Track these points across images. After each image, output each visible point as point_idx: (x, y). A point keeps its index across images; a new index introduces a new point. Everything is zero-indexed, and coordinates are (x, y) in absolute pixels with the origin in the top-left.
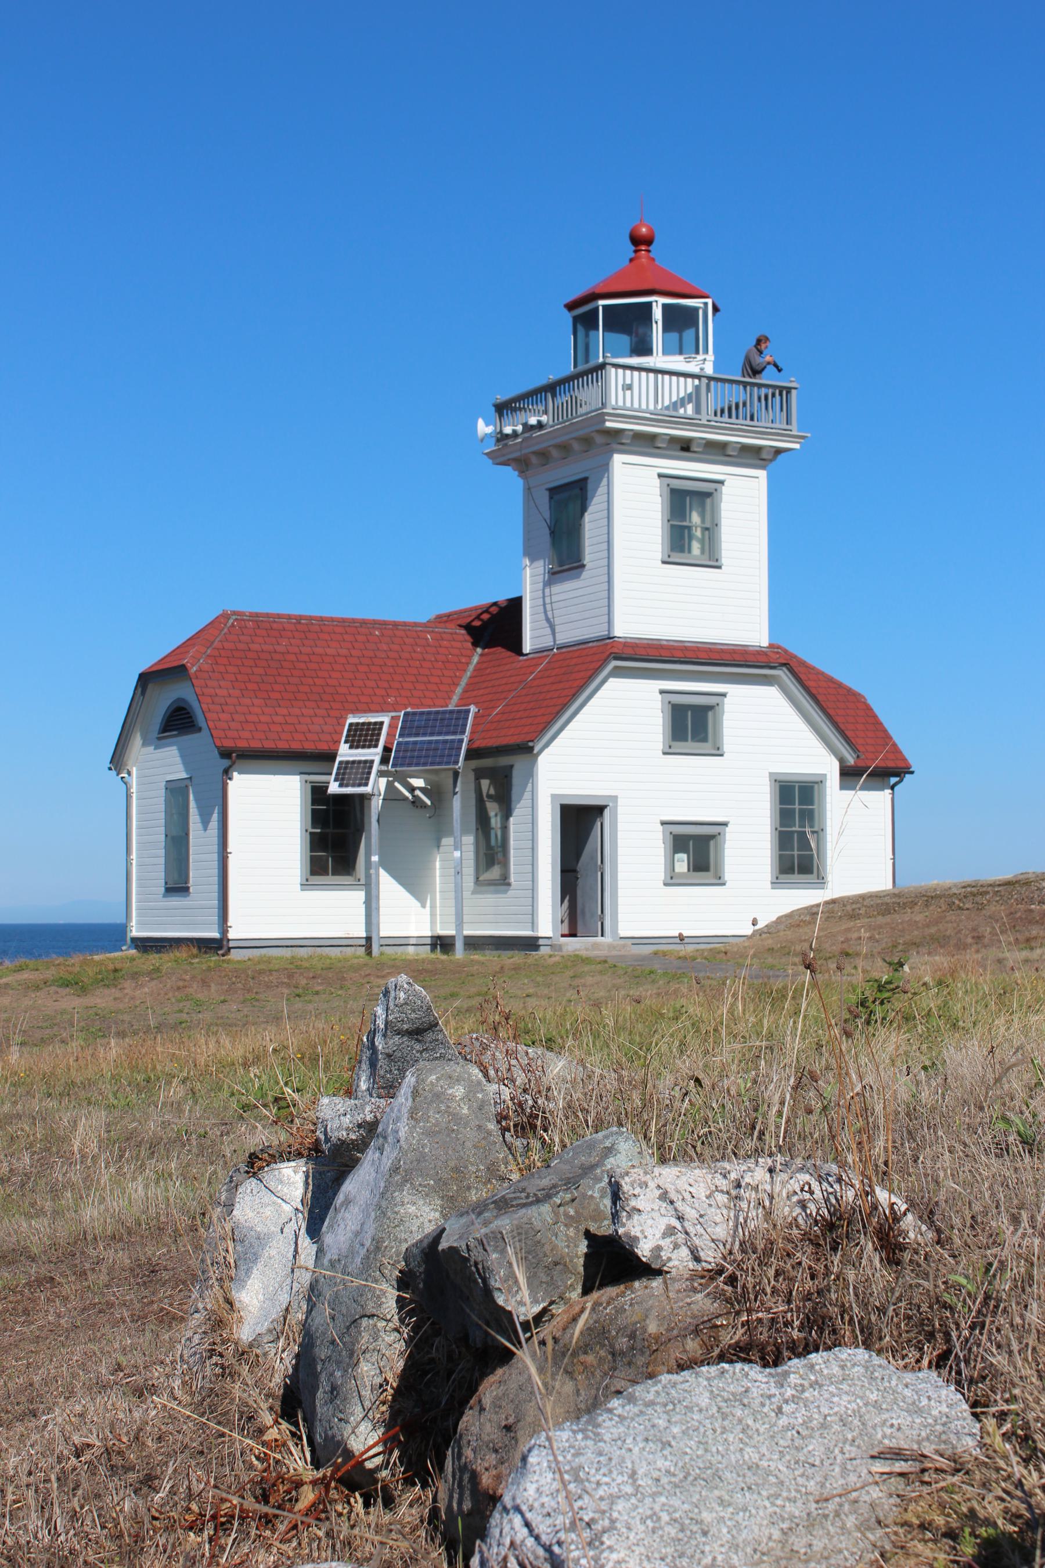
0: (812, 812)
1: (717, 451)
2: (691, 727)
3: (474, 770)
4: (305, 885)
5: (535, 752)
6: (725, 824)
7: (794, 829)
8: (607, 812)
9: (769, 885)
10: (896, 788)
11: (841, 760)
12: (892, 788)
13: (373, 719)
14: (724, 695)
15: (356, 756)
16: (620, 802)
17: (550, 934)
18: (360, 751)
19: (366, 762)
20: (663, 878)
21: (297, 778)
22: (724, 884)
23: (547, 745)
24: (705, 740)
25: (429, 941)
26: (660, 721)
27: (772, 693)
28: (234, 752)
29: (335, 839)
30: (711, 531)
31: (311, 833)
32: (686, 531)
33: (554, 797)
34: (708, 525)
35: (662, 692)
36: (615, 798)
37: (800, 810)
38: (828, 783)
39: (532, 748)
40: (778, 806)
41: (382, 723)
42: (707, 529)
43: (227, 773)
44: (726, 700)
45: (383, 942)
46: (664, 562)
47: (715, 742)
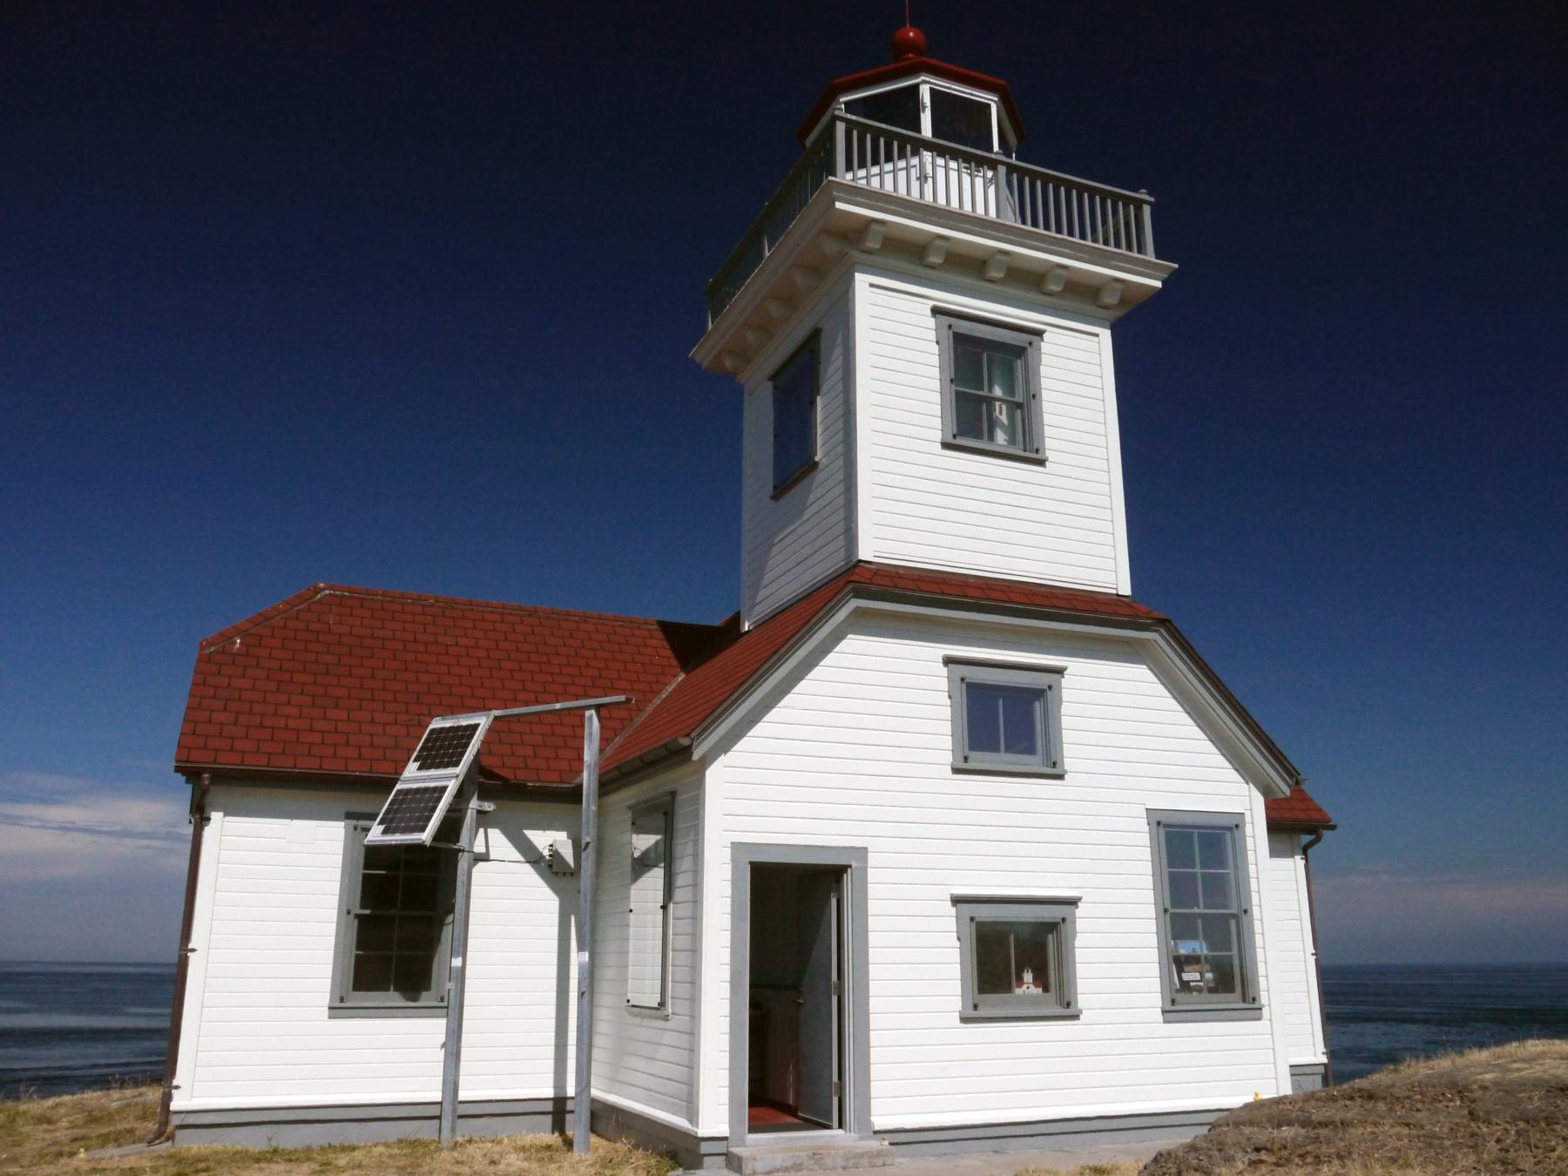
1: (1028, 282)
2: (1005, 728)
4: (339, 1009)
5: (696, 757)
6: (1073, 902)
7: (1196, 910)
8: (847, 879)
9: (1160, 1017)
10: (1309, 851)
11: (1266, 791)
12: (1304, 852)
13: (464, 721)
14: (1059, 671)
16: (872, 859)
17: (723, 1129)
18: (432, 772)
19: (435, 789)
20: (959, 1006)
21: (342, 824)
22: (1075, 1017)
23: (725, 745)
24: (1030, 750)
25: (549, 1107)
26: (946, 712)
27: (1139, 674)
28: (205, 770)
29: (399, 936)
30: (1025, 410)
31: (357, 916)
33: (737, 848)
34: (1019, 398)
35: (948, 661)
36: (862, 852)
37: (1195, 874)
38: (1248, 830)
39: (688, 750)
40: (1166, 870)
41: (476, 726)
42: (1019, 406)
43: (200, 816)
45: (462, 1110)
46: (956, 771)
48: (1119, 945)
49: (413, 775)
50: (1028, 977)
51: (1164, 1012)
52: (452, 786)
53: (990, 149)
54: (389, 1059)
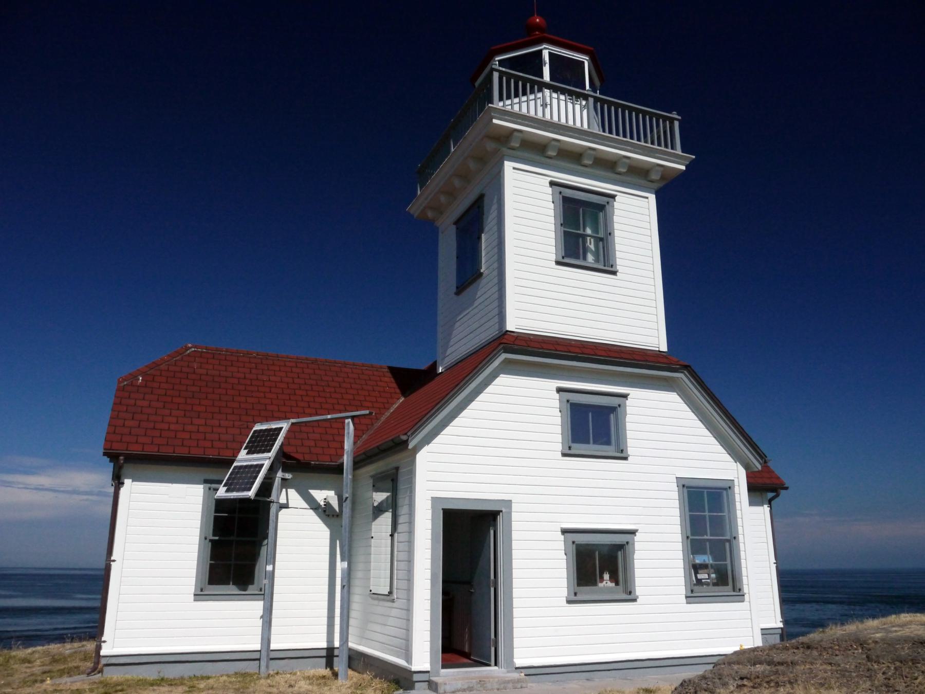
0: (721, 519)
1: (606, 167)
2: (593, 429)
3: (372, 477)
5: (410, 447)
6: (633, 532)
7: (705, 537)
8: (500, 519)
9: (685, 601)
10: (772, 502)
11: (747, 467)
12: (770, 502)
13: (274, 426)
14: (625, 396)
15: (250, 460)
16: (514, 507)
17: (426, 667)
18: (255, 456)
19: (257, 466)
20: (566, 594)
21: (202, 486)
23: (428, 440)
24: (608, 443)
25: (324, 653)
26: (558, 420)
30: (605, 242)
31: (211, 541)
32: (581, 240)
33: (435, 500)
34: (601, 235)
36: (509, 503)
37: (705, 516)
38: (736, 490)
39: (406, 443)
40: (688, 514)
41: (281, 429)
42: (601, 239)
43: (118, 482)
44: (637, 538)
45: (273, 655)
47: (618, 444)
48: (660, 558)
49: (244, 458)
50: (606, 576)
51: (686, 597)
52: (267, 464)
53: (584, 88)
54: (229, 625)
